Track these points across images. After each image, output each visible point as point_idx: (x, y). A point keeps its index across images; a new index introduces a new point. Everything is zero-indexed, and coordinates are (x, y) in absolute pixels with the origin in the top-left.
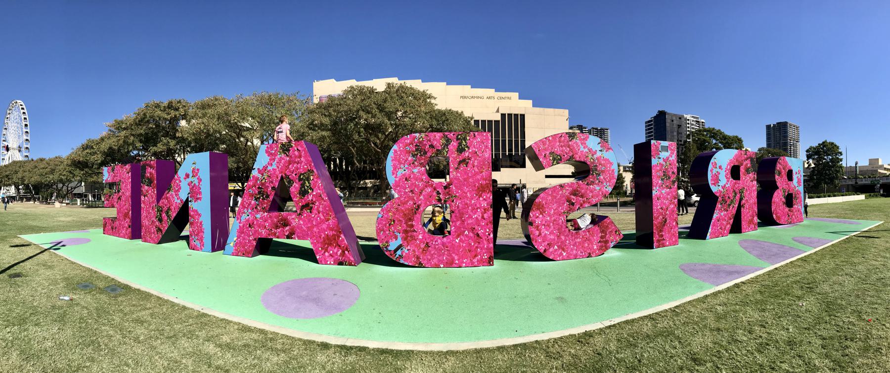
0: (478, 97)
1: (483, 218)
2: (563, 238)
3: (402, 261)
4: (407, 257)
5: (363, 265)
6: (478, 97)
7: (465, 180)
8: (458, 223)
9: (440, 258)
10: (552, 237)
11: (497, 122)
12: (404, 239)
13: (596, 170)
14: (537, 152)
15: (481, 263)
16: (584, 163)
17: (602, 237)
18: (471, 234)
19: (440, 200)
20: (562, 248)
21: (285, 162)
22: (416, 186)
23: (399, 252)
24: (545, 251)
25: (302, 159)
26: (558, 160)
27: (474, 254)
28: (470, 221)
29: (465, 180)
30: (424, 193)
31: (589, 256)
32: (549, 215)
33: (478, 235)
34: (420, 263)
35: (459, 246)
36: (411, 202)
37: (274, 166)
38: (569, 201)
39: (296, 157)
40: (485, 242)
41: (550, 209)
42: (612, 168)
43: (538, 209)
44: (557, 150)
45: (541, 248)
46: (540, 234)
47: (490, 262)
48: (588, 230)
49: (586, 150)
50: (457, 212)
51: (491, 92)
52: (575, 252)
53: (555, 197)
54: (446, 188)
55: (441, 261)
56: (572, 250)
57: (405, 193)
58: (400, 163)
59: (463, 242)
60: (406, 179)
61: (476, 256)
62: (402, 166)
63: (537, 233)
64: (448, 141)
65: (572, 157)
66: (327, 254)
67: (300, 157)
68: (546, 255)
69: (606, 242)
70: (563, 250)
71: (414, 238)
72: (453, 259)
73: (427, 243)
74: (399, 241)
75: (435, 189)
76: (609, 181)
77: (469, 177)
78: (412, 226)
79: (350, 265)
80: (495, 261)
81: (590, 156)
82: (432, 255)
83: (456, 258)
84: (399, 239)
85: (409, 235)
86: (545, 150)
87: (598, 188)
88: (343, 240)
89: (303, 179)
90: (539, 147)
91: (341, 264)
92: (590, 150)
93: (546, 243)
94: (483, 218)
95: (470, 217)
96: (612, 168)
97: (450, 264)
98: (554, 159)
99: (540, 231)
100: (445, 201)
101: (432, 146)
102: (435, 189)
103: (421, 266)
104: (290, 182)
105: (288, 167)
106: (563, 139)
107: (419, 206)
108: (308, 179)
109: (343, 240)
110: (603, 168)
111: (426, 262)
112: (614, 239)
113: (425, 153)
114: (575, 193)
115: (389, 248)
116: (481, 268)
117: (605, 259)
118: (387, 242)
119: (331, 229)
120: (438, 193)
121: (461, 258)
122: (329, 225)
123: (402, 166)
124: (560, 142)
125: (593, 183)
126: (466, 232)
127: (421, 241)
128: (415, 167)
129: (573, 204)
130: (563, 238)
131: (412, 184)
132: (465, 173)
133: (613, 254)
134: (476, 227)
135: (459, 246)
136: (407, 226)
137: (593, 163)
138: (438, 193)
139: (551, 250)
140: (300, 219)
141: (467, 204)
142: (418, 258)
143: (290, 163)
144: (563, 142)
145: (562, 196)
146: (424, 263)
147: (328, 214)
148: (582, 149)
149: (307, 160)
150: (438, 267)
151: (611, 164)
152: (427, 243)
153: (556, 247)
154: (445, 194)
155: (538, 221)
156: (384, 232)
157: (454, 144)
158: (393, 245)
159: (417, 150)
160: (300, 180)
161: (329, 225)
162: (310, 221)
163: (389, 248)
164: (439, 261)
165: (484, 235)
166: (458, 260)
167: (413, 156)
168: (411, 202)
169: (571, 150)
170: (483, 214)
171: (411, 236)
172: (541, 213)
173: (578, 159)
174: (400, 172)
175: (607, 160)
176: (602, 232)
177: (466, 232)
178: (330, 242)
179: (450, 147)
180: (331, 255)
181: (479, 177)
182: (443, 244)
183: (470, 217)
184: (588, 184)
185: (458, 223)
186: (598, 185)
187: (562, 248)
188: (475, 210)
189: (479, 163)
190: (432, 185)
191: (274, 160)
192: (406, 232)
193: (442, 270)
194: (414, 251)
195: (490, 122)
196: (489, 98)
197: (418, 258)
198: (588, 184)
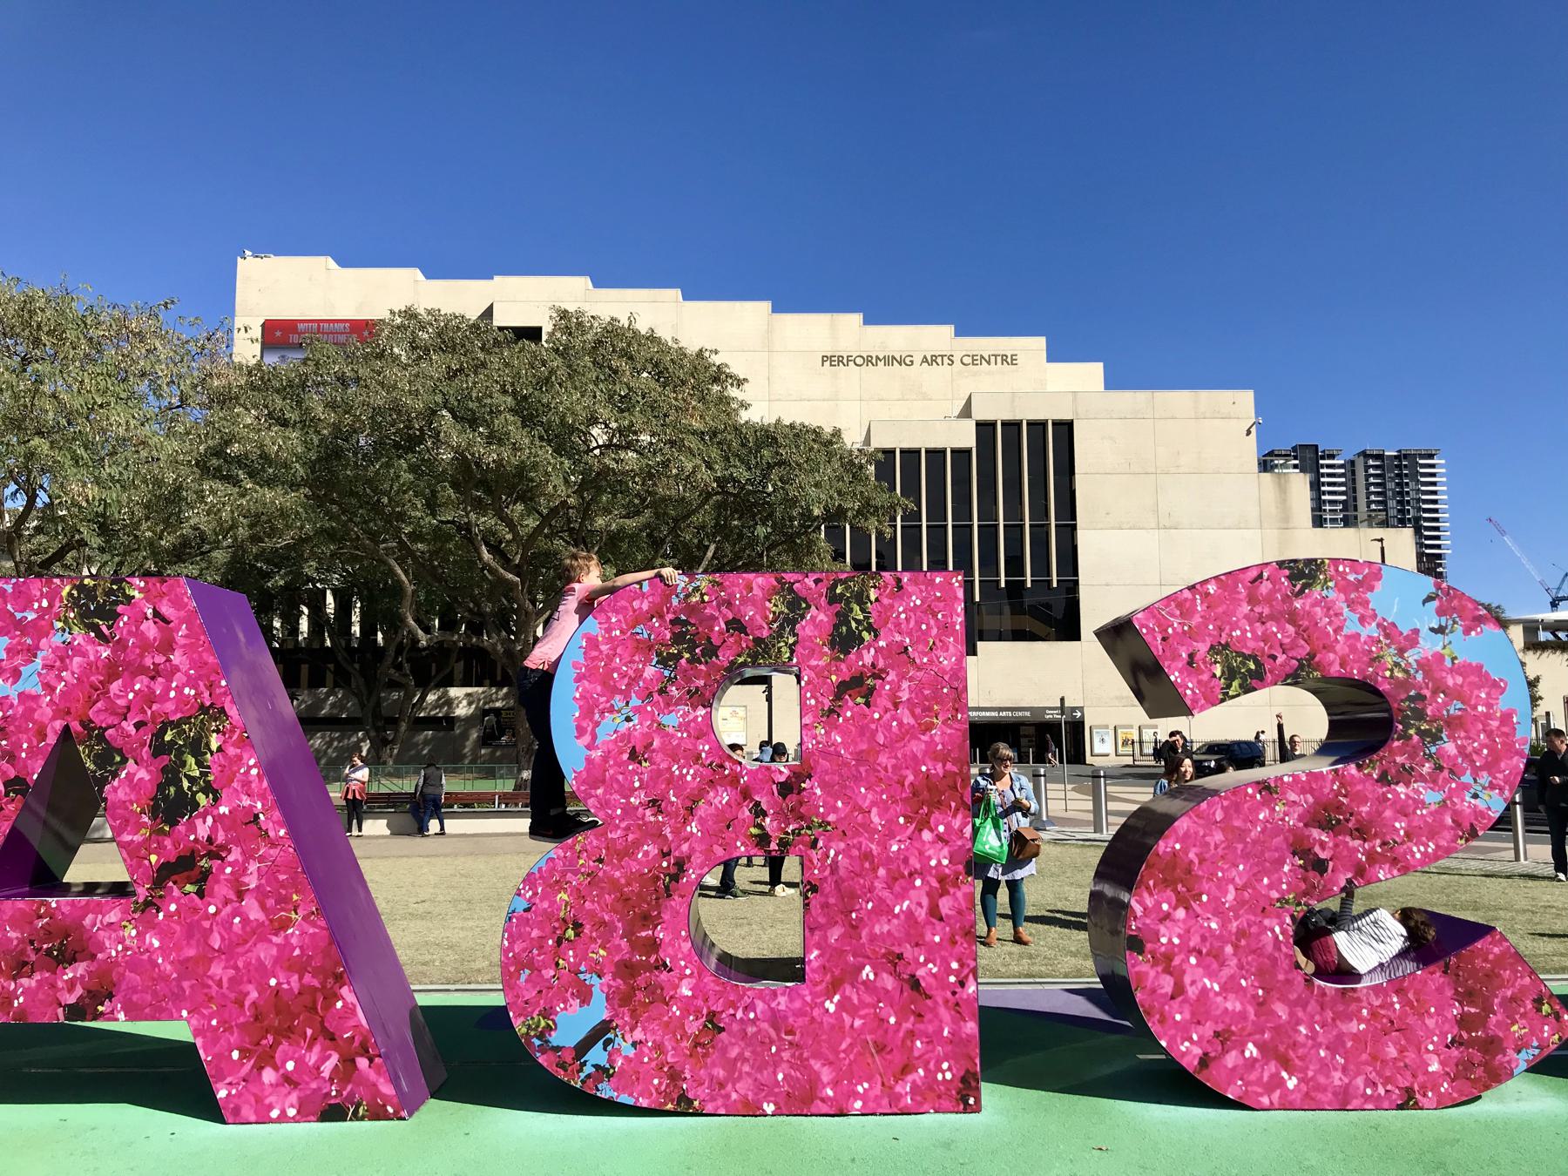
0: (889, 360)
1: (934, 912)
2: (1282, 1011)
3: (606, 1091)
4: (633, 1075)
5: (434, 1109)
6: (889, 360)
7: (860, 758)
8: (834, 935)
9: (764, 1077)
10: (1233, 1005)
11: (961, 455)
12: (619, 999)
13: (1420, 715)
14: (1157, 646)
15: (929, 1098)
16: (1366, 687)
17: (1463, 1022)
18: (889, 982)
19: (763, 840)
20: (1279, 1052)
21: (90, 667)
22: (671, 781)
23: (597, 1055)
24: (1205, 1061)
25: (177, 658)
26: (1249, 676)
27: (898, 1058)
28: (881, 928)
29: (860, 758)
30: (702, 809)
31: (1408, 1101)
32: (1218, 910)
33: (915, 983)
34: (684, 1099)
35: (838, 1028)
36: (650, 848)
37: (30, 681)
38: (1301, 849)
39: (145, 645)
40: (944, 1014)
41: (1222, 885)
42: (1503, 704)
43: (1167, 883)
44: (1243, 633)
45: (1188, 1051)
46: (1179, 990)
47: (964, 1098)
48: (1398, 987)
49: (1372, 630)
50: (828, 887)
51: (939, 337)
52: (1337, 1078)
53: (1242, 834)
54: (786, 788)
55: (766, 1090)
56: (1325, 1067)
57: (629, 810)
58: (612, 690)
59: (854, 1012)
60: (634, 756)
61: (906, 1069)
62: (618, 702)
63: (1167, 983)
64: (797, 605)
65: (1309, 662)
66: (927, 836)
67: (167, 646)
68: (1210, 1079)
69: (1491, 1046)
70: (1286, 1064)
71: (661, 997)
72: (814, 1082)
73: (712, 1016)
74: (598, 1010)
75: (746, 794)
76: (1490, 766)
77: (877, 749)
78: (653, 945)
79: (377, 1114)
80: (990, 1093)
81: (1390, 657)
82: (731, 1066)
83: (826, 1075)
84: (599, 998)
85: (638, 985)
86: (1191, 635)
87: (1432, 797)
88: (349, 1010)
89: (173, 744)
90: (1163, 625)
91: (334, 1113)
92: (1389, 630)
93: (1208, 1029)
94: (934, 912)
95: (884, 910)
96: (1503, 704)
97: (800, 1102)
98: (1230, 674)
99: (1178, 975)
100: (783, 844)
101: (736, 625)
102: (746, 794)
103: (685, 1107)
104: (110, 758)
105: (102, 690)
106: (1265, 587)
107: (681, 865)
108: (198, 747)
109: (349, 1010)
110: (1455, 708)
111: (704, 1091)
112: (1531, 1035)
113: (711, 651)
114: (1327, 815)
115: (555, 1039)
116: (930, 1119)
117: (1489, 1125)
118: (548, 1013)
119: (300, 967)
120: (759, 812)
121: (846, 1078)
122: (286, 947)
123: (618, 702)
124: (1252, 600)
125: (1406, 775)
126: (867, 972)
127: (688, 1006)
128: (670, 704)
129: (1320, 866)
130: (1282, 1011)
131: (657, 774)
132: (862, 731)
133: (1523, 1101)
134: (908, 951)
135: (838, 1028)
136: (635, 945)
137: (1405, 685)
138: (759, 812)
139: (1231, 1059)
140: (147, 925)
141: (868, 856)
142: (675, 1076)
143: (112, 670)
144: (1269, 599)
145: (1272, 829)
146: (699, 1095)
147: (285, 900)
148: (1352, 625)
149: (199, 664)
150: (754, 1111)
151: (1496, 687)
152: (712, 1016)
153: (1251, 1050)
154: (781, 816)
155: (1168, 937)
156: (536, 969)
157: (818, 617)
158: (571, 1025)
159: (678, 639)
160: (160, 748)
161: (286, 947)
162: (194, 929)
163: (555, 1039)
164: (760, 1087)
165: (944, 984)
166: (835, 1084)
167: (663, 662)
168: (650, 848)
169: (1301, 632)
170: (934, 897)
171: (649, 989)
172: (1182, 901)
173: (1335, 670)
174: (610, 727)
175: (1476, 674)
176: (1467, 997)
177: (867, 972)
178: (276, 1024)
179: (805, 628)
180: (939, 838)
181: (917, 747)
182: (775, 1019)
183: (884, 910)
184: (1383, 779)
185: (834, 935)
186: (1433, 781)
187: (1279, 1052)
188: (900, 880)
189: (917, 690)
190: (734, 780)
191: (32, 652)
192: (627, 969)
193: (771, 1127)
194: (658, 1046)
195: (936, 455)
196: (931, 360)
197: (675, 1076)
198: (1383, 779)
